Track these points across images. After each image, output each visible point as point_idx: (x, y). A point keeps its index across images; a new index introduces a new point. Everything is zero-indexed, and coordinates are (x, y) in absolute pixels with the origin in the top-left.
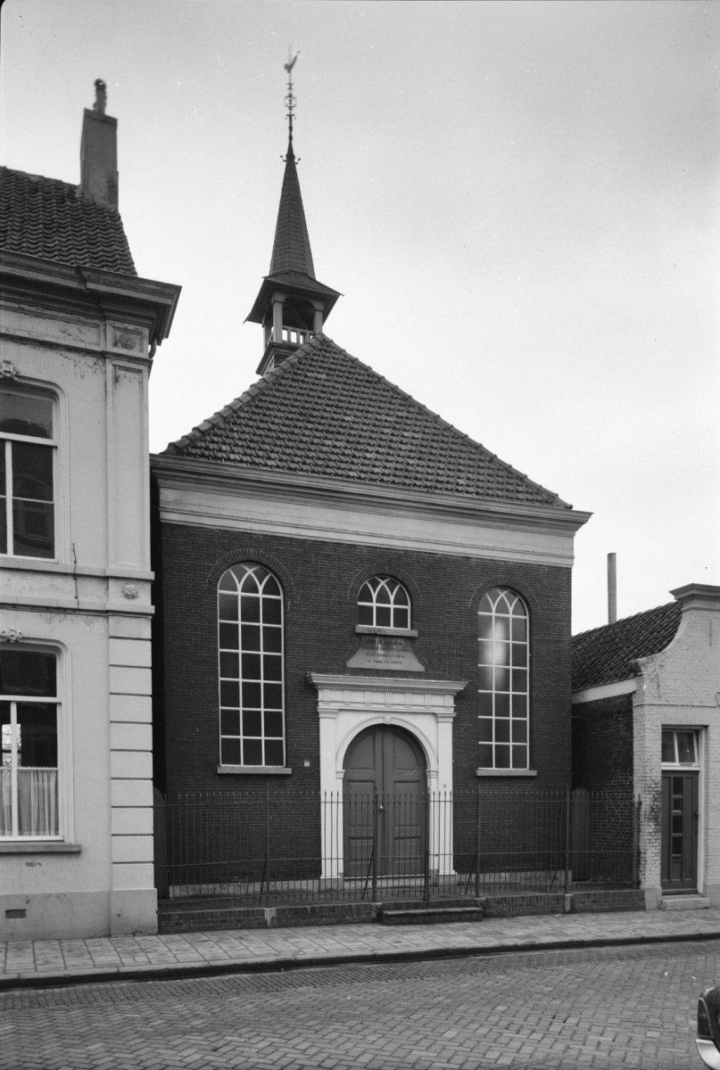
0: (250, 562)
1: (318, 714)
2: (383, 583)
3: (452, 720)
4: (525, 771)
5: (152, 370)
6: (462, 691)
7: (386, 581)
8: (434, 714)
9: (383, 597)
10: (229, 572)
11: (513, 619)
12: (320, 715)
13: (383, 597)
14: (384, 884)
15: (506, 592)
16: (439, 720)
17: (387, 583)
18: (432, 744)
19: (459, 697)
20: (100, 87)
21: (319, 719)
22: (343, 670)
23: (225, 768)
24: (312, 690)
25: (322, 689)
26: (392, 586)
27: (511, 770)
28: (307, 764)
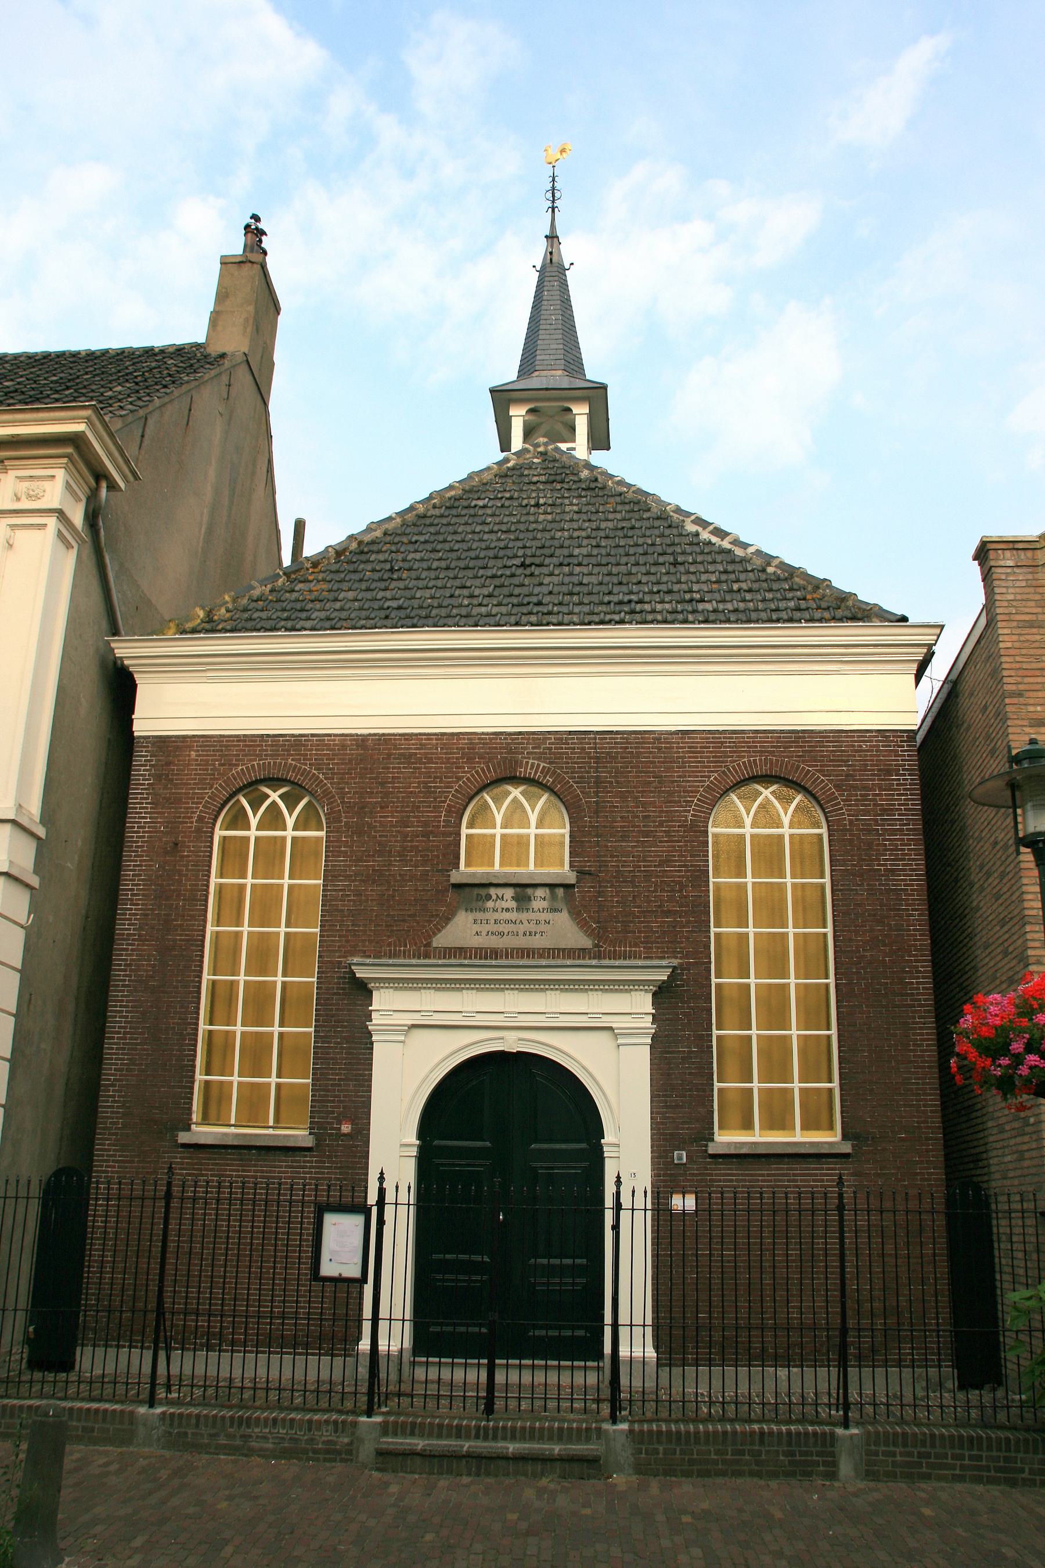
0: (274, 782)
1: (370, 1034)
2: (274, 796)
3: (649, 1041)
4: (829, 1138)
5: (867, 595)
6: (664, 982)
7: (771, 789)
8: (611, 1029)
9: (273, 818)
10: (238, 801)
11: (752, 836)
12: (374, 1038)
13: (273, 818)
14: (514, 1377)
15: (522, 788)
16: (620, 1041)
17: (281, 797)
18: (608, 1092)
19: (662, 994)
20: (254, 233)
21: (372, 1043)
22: (426, 952)
23: (203, 1132)
24: (363, 990)
25: (378, 988)
26: (291, 800)
27: (799, 1137)
28: (346, 1128)
